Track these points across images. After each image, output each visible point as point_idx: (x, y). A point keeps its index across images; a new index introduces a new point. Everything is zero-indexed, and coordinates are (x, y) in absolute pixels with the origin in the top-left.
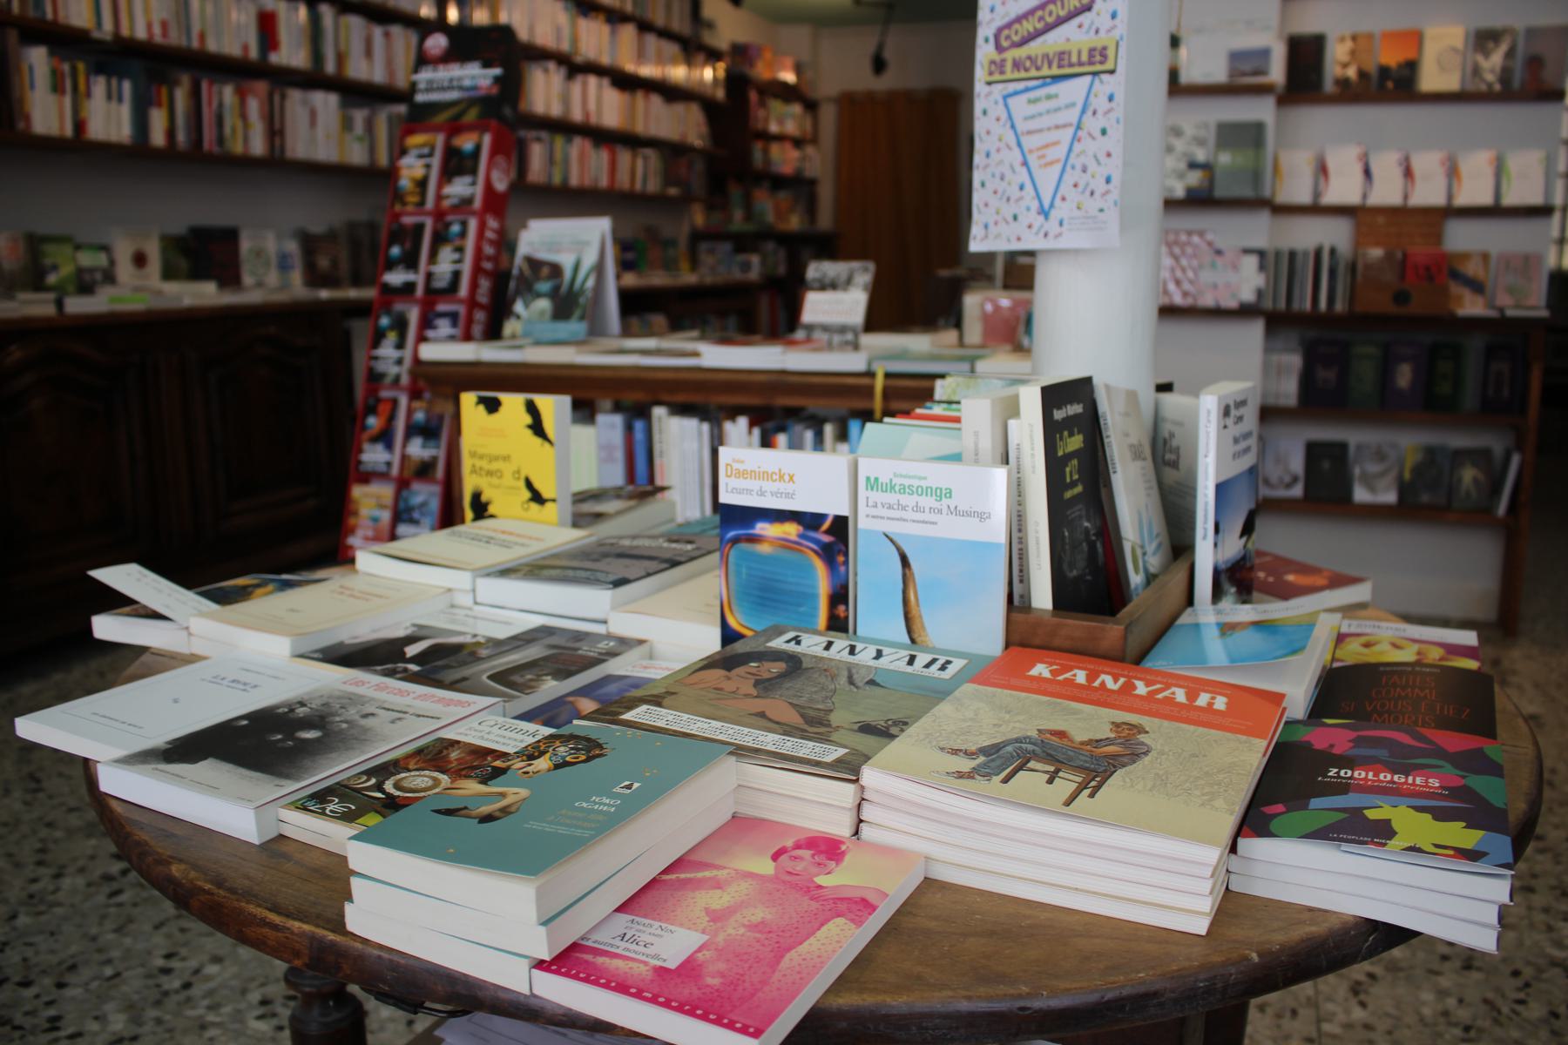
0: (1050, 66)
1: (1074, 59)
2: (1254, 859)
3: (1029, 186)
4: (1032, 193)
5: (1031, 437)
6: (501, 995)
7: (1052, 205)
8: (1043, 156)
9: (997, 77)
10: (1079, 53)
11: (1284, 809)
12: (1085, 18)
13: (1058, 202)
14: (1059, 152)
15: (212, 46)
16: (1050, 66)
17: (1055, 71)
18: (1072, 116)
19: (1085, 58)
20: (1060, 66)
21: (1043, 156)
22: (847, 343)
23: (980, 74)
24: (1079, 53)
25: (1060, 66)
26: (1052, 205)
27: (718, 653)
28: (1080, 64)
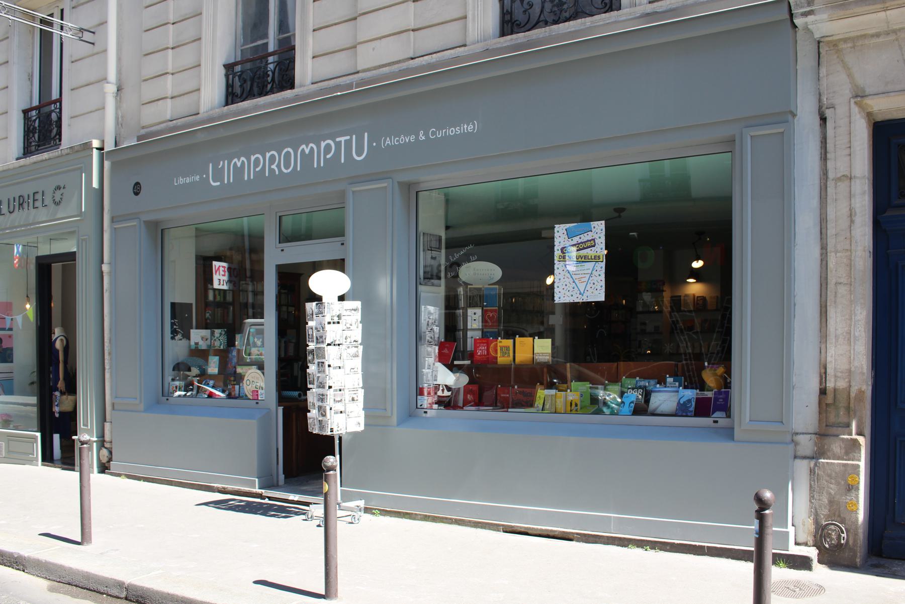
0: (581, 259)
1: (590, 257)
2: (814, 434)
3: (576, 288)
4: (577, 289)
5: (7, 403)
6: (277, 370)
7: (584, 292)
8: (580, 280)
9: (562, 260)
10: (591, 256)
11: (725, 416)
12: (593, 249)
13: (586, 291)
14: (586, 279)
15: (323, 513)
16: (581, 259)
17: (583, 260)
18: (590, 271)
19: (593, 258)
20: (584, 259)
21: (580, 280)
22: (322, 366)
23: (556, 259)
24: (591, 256)
25: (584, 259)
26: (584, 292)
27: (207, 372)
28: (591, 259)
